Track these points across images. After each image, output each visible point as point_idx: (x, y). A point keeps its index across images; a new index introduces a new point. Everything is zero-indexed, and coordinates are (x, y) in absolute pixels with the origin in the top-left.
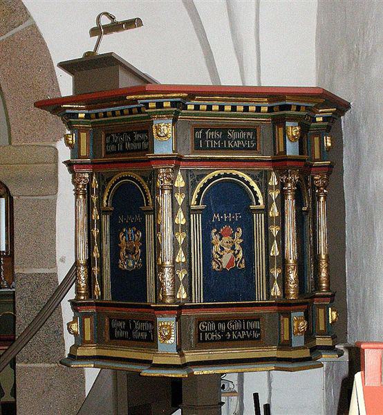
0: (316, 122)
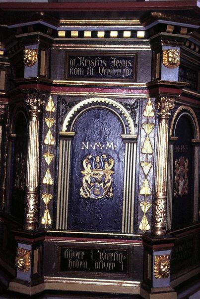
0: (137, 38)
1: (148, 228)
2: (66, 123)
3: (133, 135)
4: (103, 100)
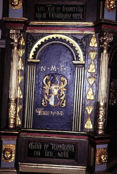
1: (91, 127)
2: (32, 53)
3: (82, 60)
4: (59, 36)
